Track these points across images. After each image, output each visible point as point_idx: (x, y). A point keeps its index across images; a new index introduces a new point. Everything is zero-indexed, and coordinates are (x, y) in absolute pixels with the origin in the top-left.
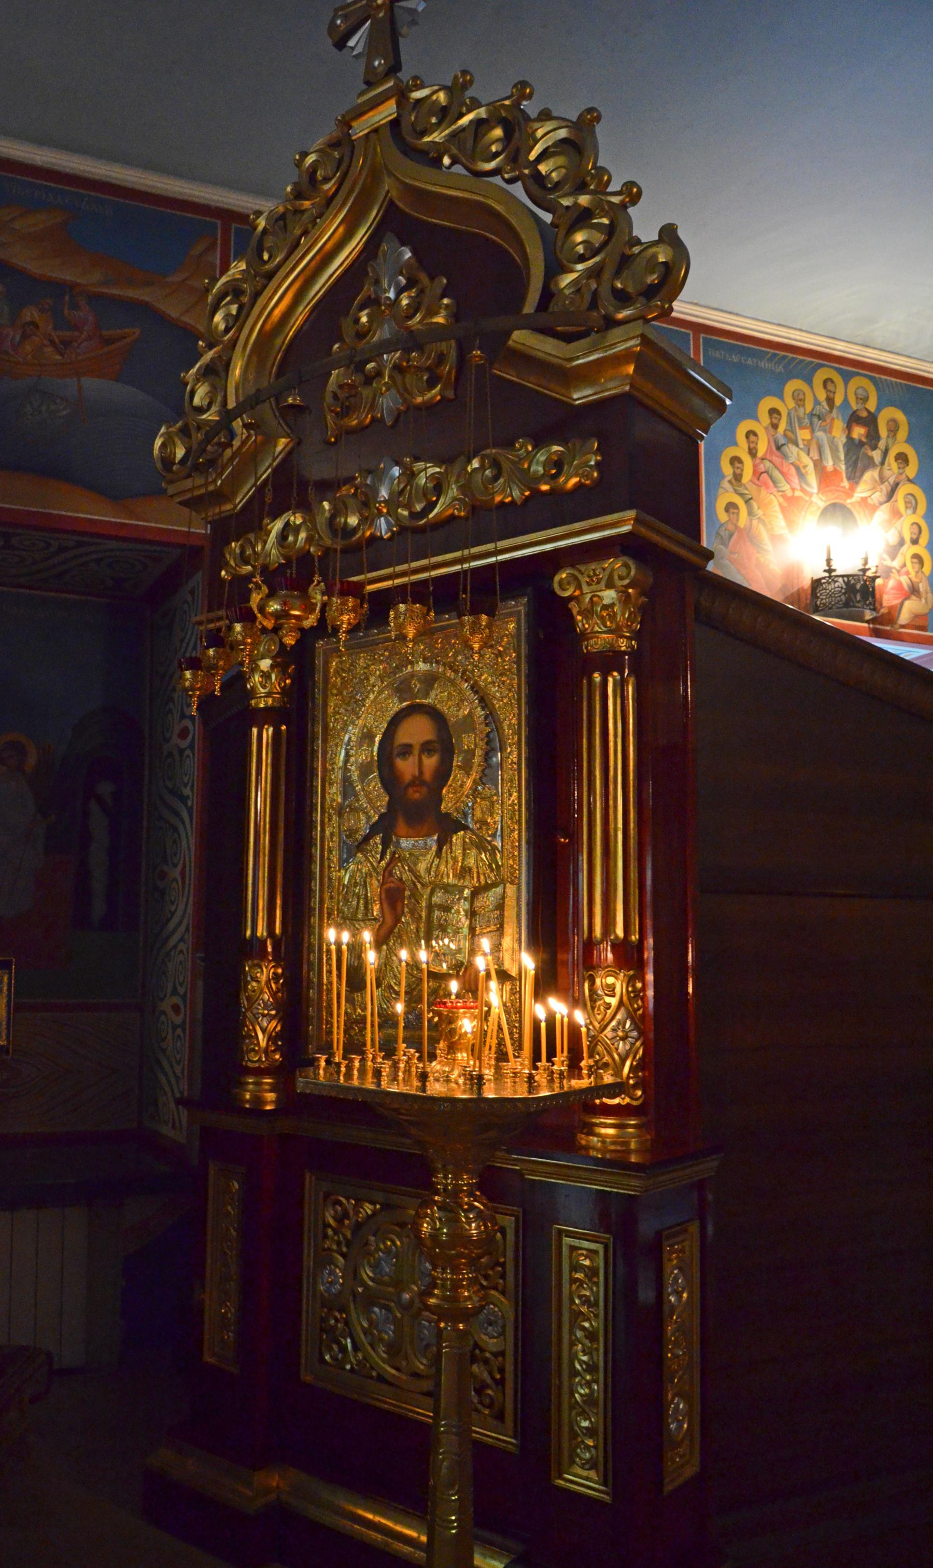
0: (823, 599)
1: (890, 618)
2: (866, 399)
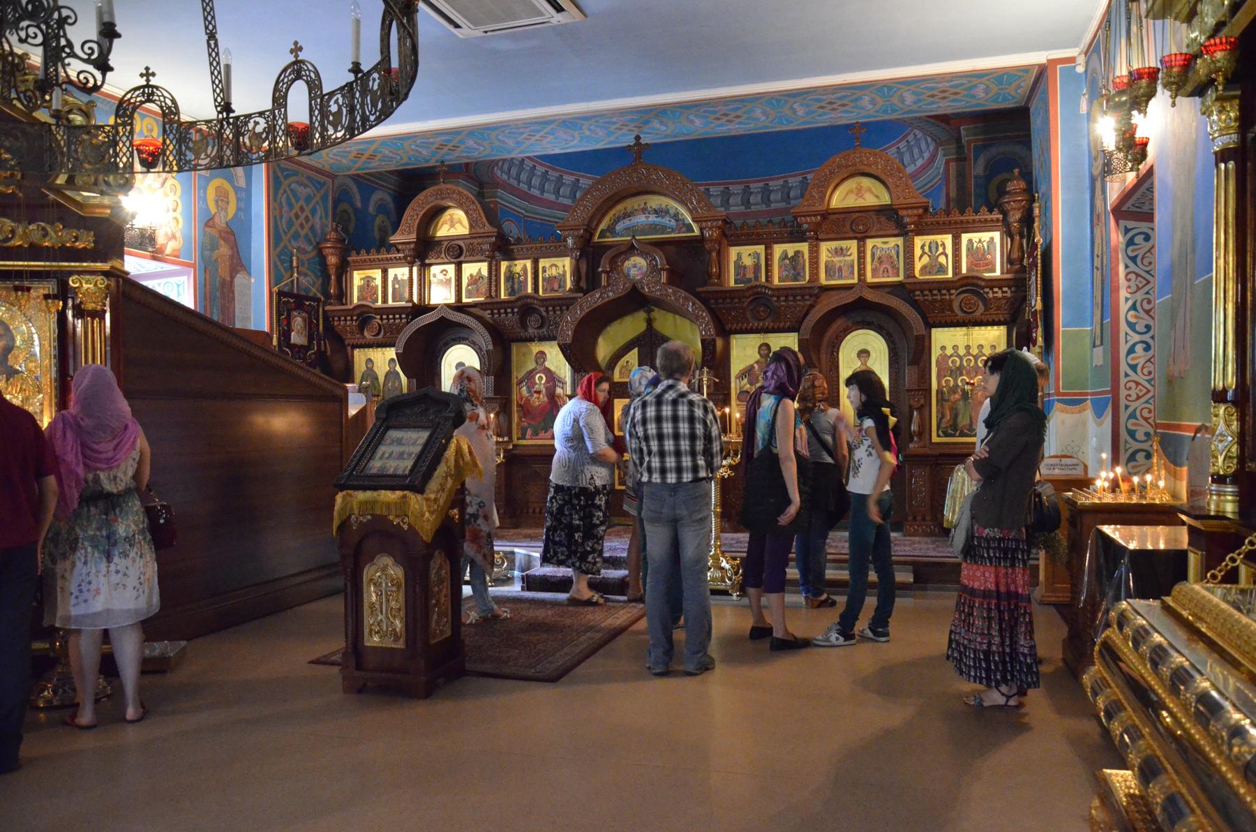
0: (1064, 597)
1: (161, 251)
2: (152, 130)
